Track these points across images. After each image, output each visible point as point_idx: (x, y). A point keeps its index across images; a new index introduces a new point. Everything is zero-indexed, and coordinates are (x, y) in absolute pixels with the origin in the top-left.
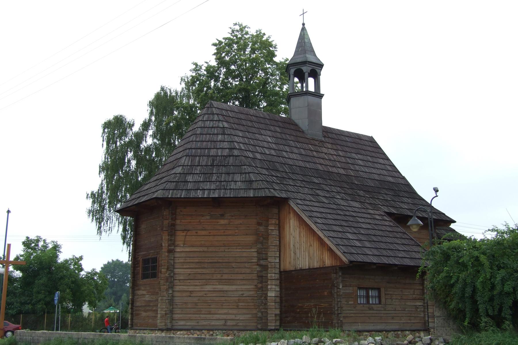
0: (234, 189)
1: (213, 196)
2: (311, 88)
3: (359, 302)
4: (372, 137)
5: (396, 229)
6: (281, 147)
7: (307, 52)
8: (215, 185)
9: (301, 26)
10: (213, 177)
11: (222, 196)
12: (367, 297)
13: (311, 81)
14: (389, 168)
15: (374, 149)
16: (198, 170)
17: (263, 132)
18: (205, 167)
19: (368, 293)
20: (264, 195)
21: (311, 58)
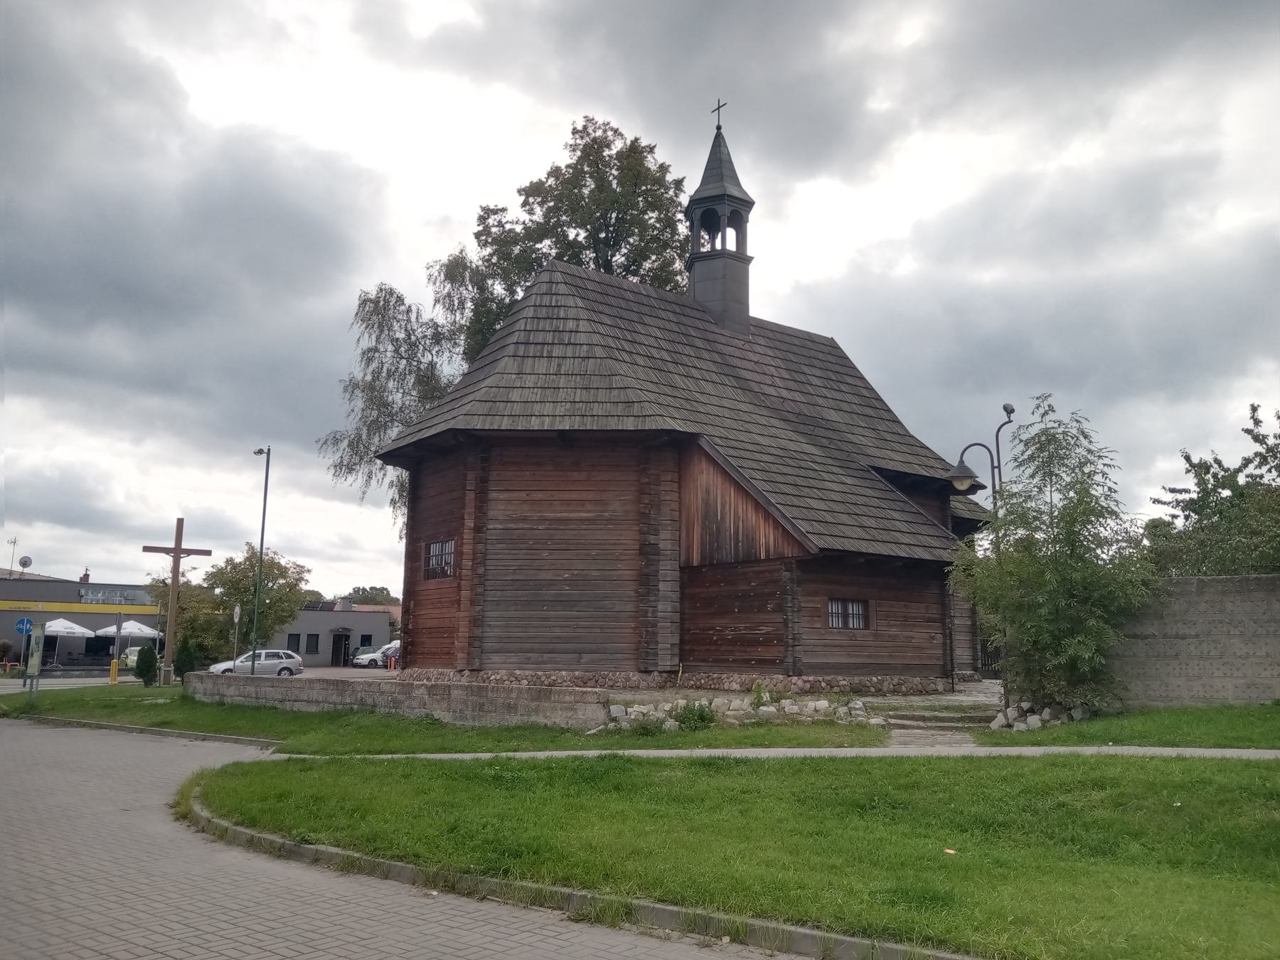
0: (598, 416)
1: (560, 428)
2: (731, 245)
3: (831, 626)
4: (832, 338)
5: (892, 496)
6: (680, 348)
7: (724, 178)
8: (563, 409)
9: (715, 131)
10: (560, 394)
11: (576, 428)
12: (845, 616)
13: (731, 233)
14: (866, 393)
15: (839, 360)
16: (530, 381)
17: (647, 320)
18: (544, 377)
19: (845, 609)
20: (654, 428)
21: (733, 191)
